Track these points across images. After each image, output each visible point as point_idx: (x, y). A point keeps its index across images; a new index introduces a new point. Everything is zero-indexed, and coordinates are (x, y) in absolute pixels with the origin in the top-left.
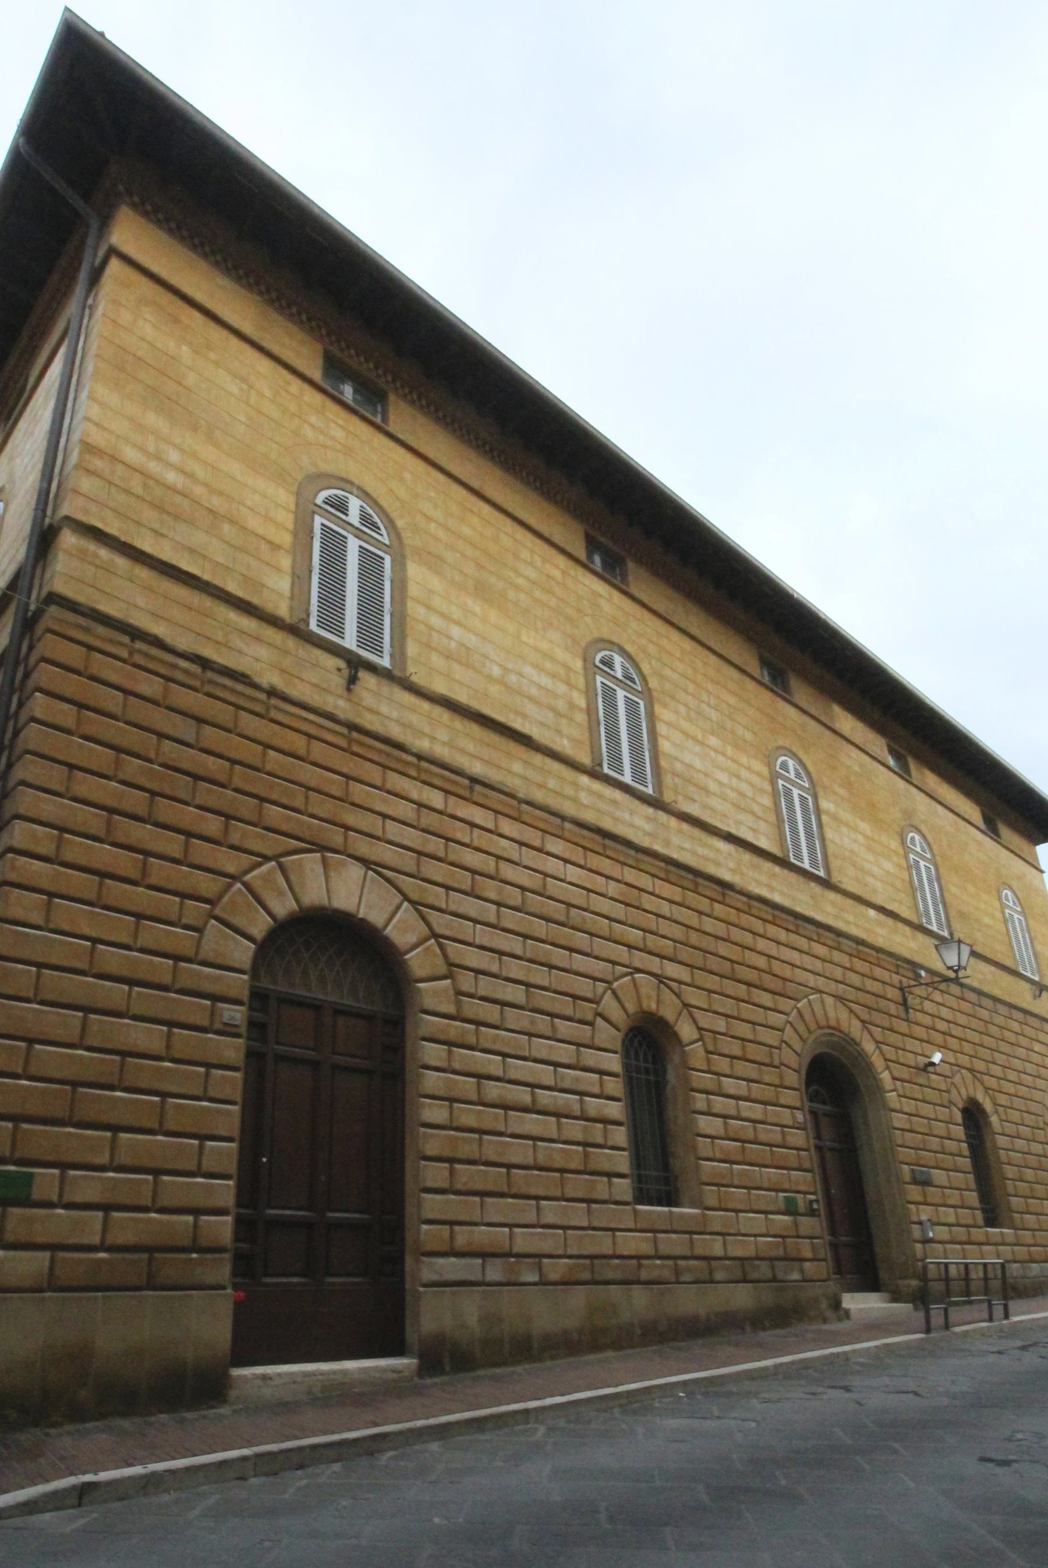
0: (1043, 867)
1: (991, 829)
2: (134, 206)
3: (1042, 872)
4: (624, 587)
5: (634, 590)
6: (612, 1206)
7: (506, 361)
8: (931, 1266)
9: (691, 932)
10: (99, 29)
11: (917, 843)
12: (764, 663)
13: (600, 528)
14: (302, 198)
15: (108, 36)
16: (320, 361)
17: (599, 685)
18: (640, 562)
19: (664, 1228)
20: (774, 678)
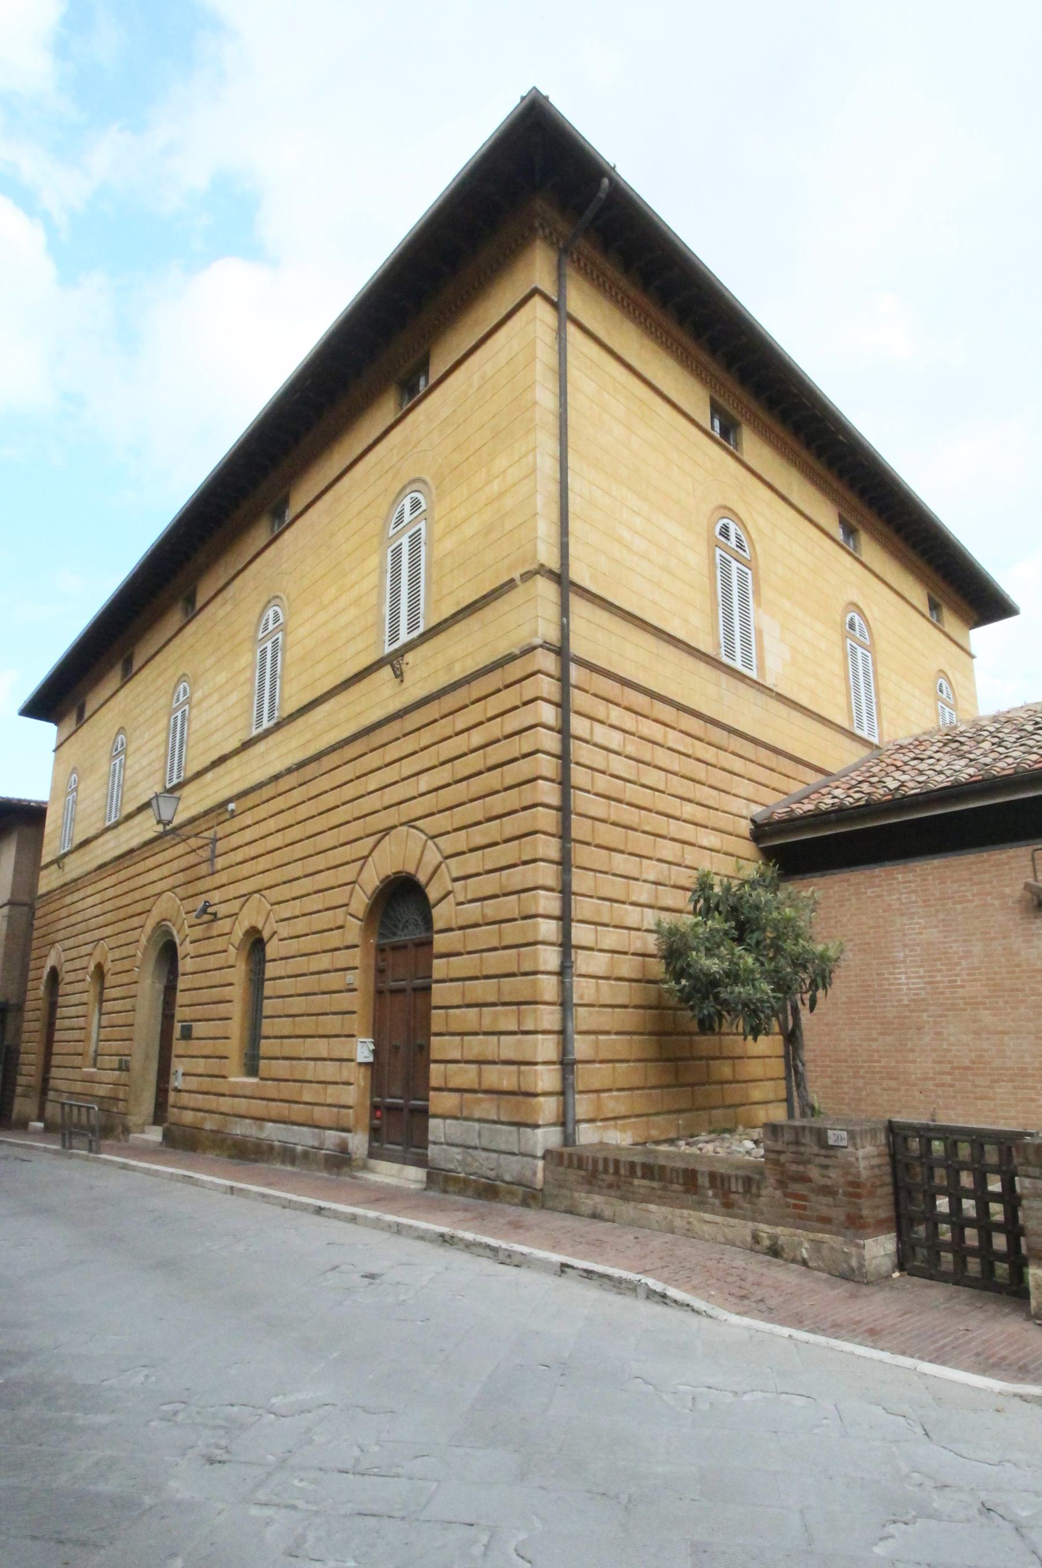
0: (973, 652)
1: (728, 432)
2: (545, 238)
3: (972, 657)
4: (857, 555)
5: (947, 629)
6: (598, 1065)
7: (678, 242)
8: (399, 1093)
9: (597, 725)
10: (544, 94)
11: (857, 628)
12: (716, 409)
13: (579, 260)
14: (862, 440)
15: (551, 100)
16: (927, 603)
17: (718, 558)
18: (866, 530)
19: (334, 1080)
20: (725, 432)
